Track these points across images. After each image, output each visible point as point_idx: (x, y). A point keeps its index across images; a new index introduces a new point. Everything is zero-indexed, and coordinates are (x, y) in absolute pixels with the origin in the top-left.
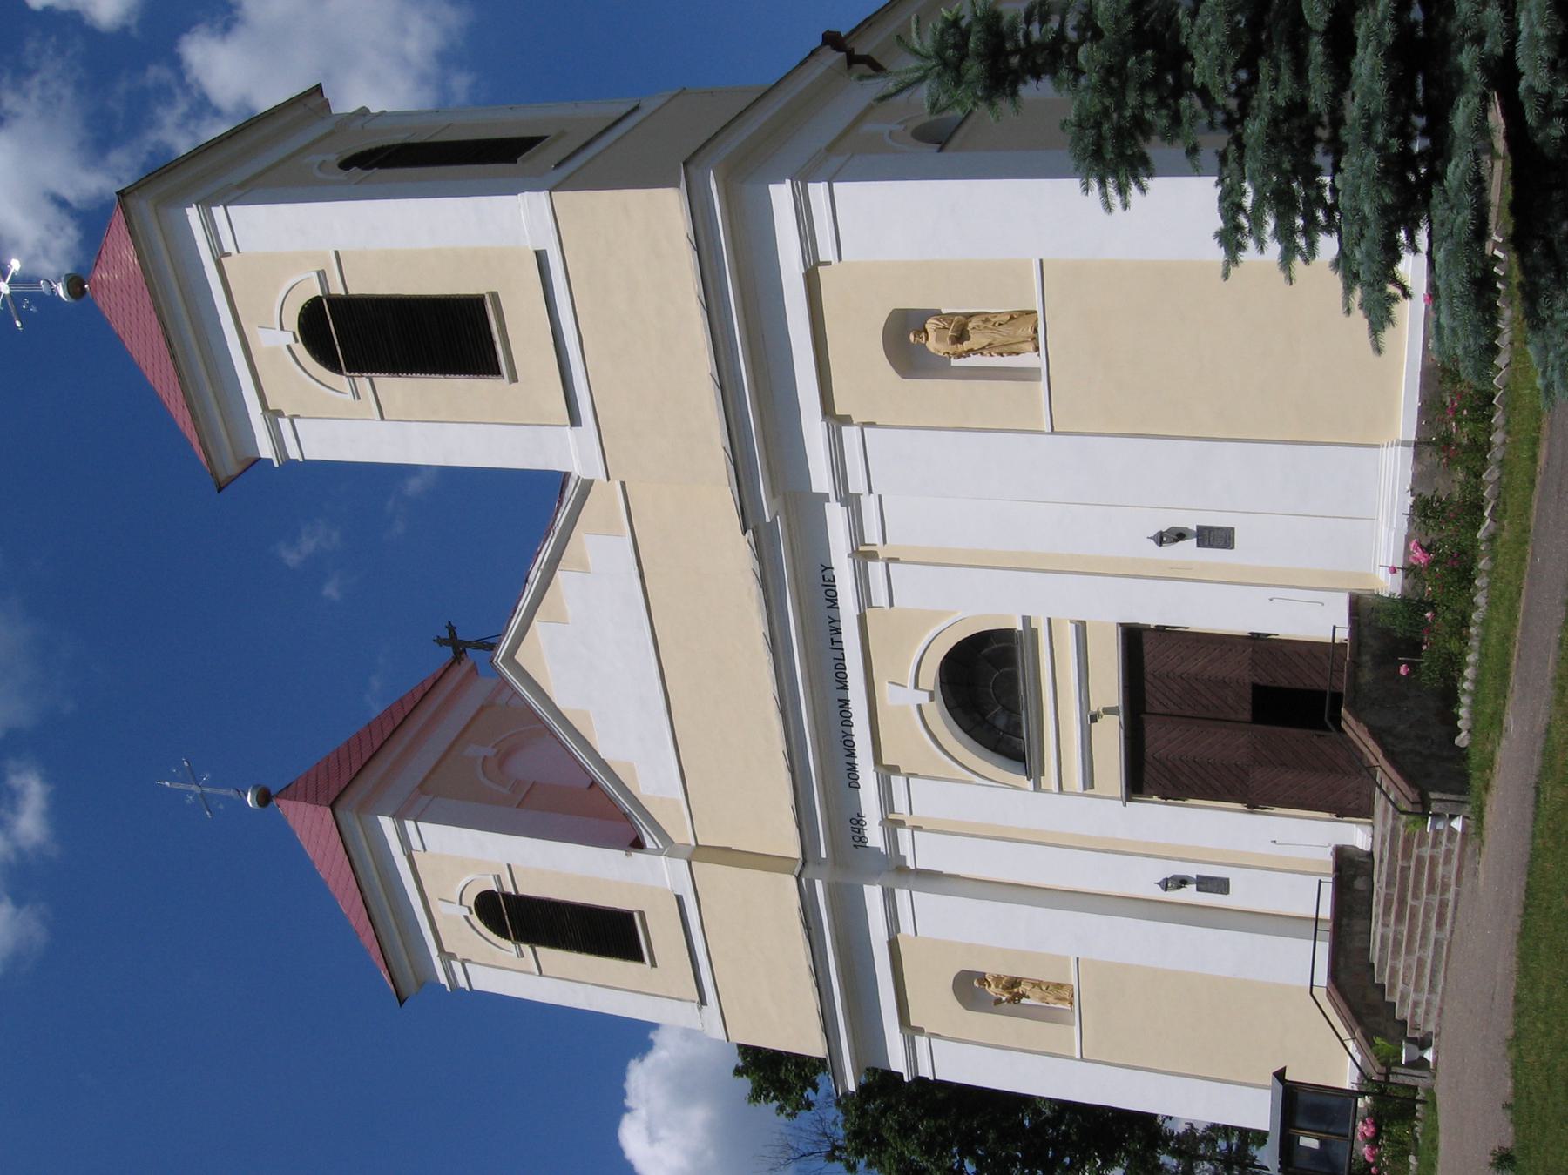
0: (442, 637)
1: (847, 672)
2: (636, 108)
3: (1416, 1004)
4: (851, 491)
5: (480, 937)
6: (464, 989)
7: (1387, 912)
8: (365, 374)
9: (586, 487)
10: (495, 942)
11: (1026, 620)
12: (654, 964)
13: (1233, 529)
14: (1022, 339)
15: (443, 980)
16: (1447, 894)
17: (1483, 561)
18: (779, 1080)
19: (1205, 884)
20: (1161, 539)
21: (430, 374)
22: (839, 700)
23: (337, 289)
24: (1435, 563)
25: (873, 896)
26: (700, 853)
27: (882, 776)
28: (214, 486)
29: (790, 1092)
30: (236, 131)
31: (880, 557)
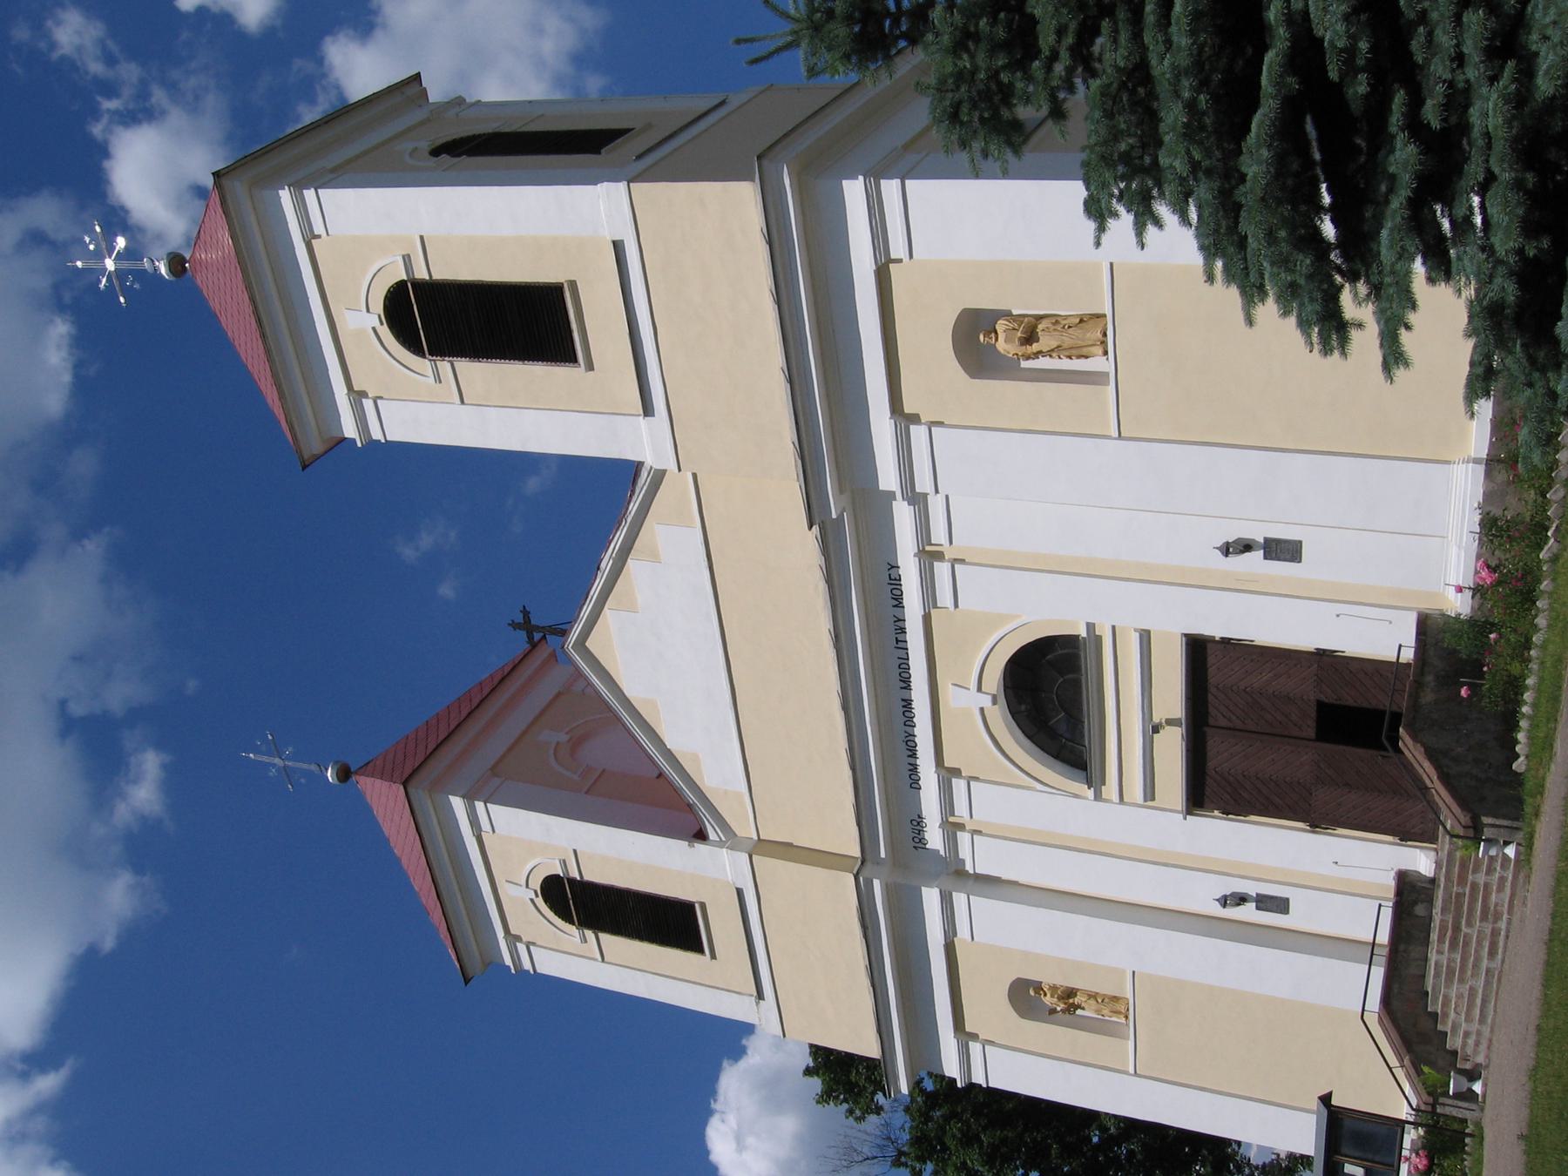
0: (516, 621)
1: (911, 672)
2: (722, 103)
3: (1467, 1034)
4: (917, 490)
5: (546, 922)
6: (528, 971)
7: (1441, 939)
8: (446, 358)
9: (659, 476)
10: (559, 927)
11: (1090, 627)
12: (713, 956)
13: (1301, 542)
14: (1090, 343)
15: (508, 961)
16: (1500, 922)
17: (1545, 583)
18: (850, 1082)
19: (1266, 903)
20: (1227, 550)
21: (510, 360)
22: (903, 700)
23: (421, 274)
24: (1499, 583)
25: (931, 898)
26: (762, 847)
27: (943, 777)
28: (299, 463)
29: (859, 1094)
30: (334, 116)
31: (946, 558)
